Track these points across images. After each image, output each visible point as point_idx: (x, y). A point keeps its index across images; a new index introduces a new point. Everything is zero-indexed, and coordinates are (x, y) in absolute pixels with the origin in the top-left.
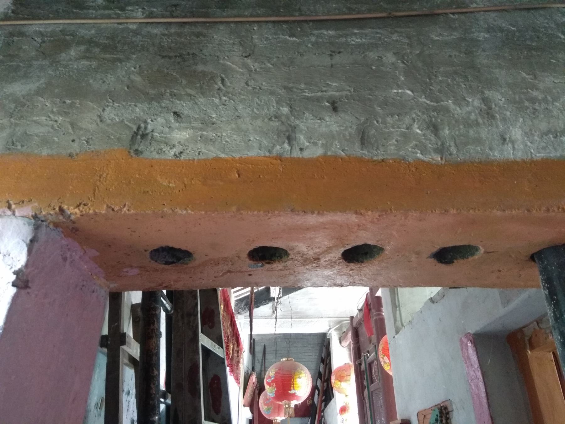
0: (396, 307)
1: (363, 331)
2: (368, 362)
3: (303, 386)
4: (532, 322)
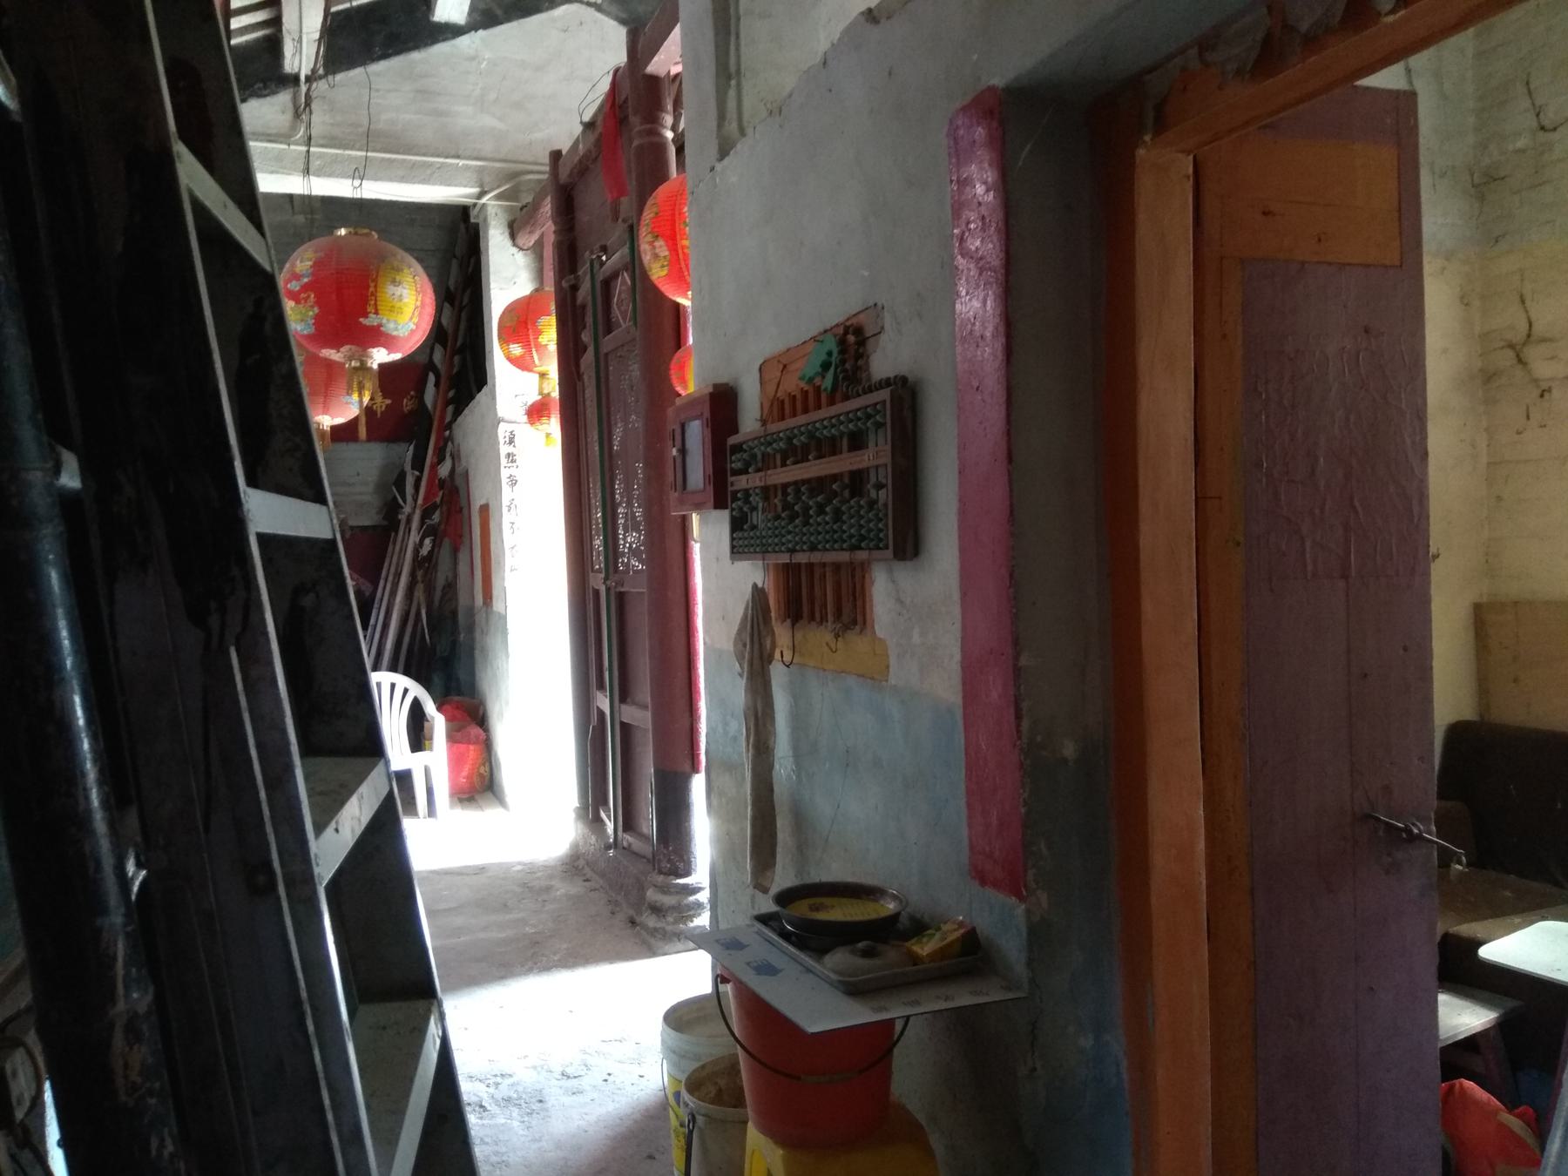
0: (729, 78)
1: (595, 198)
2: (602, 274)
3: (408, 310)
4: (1182, 51)
